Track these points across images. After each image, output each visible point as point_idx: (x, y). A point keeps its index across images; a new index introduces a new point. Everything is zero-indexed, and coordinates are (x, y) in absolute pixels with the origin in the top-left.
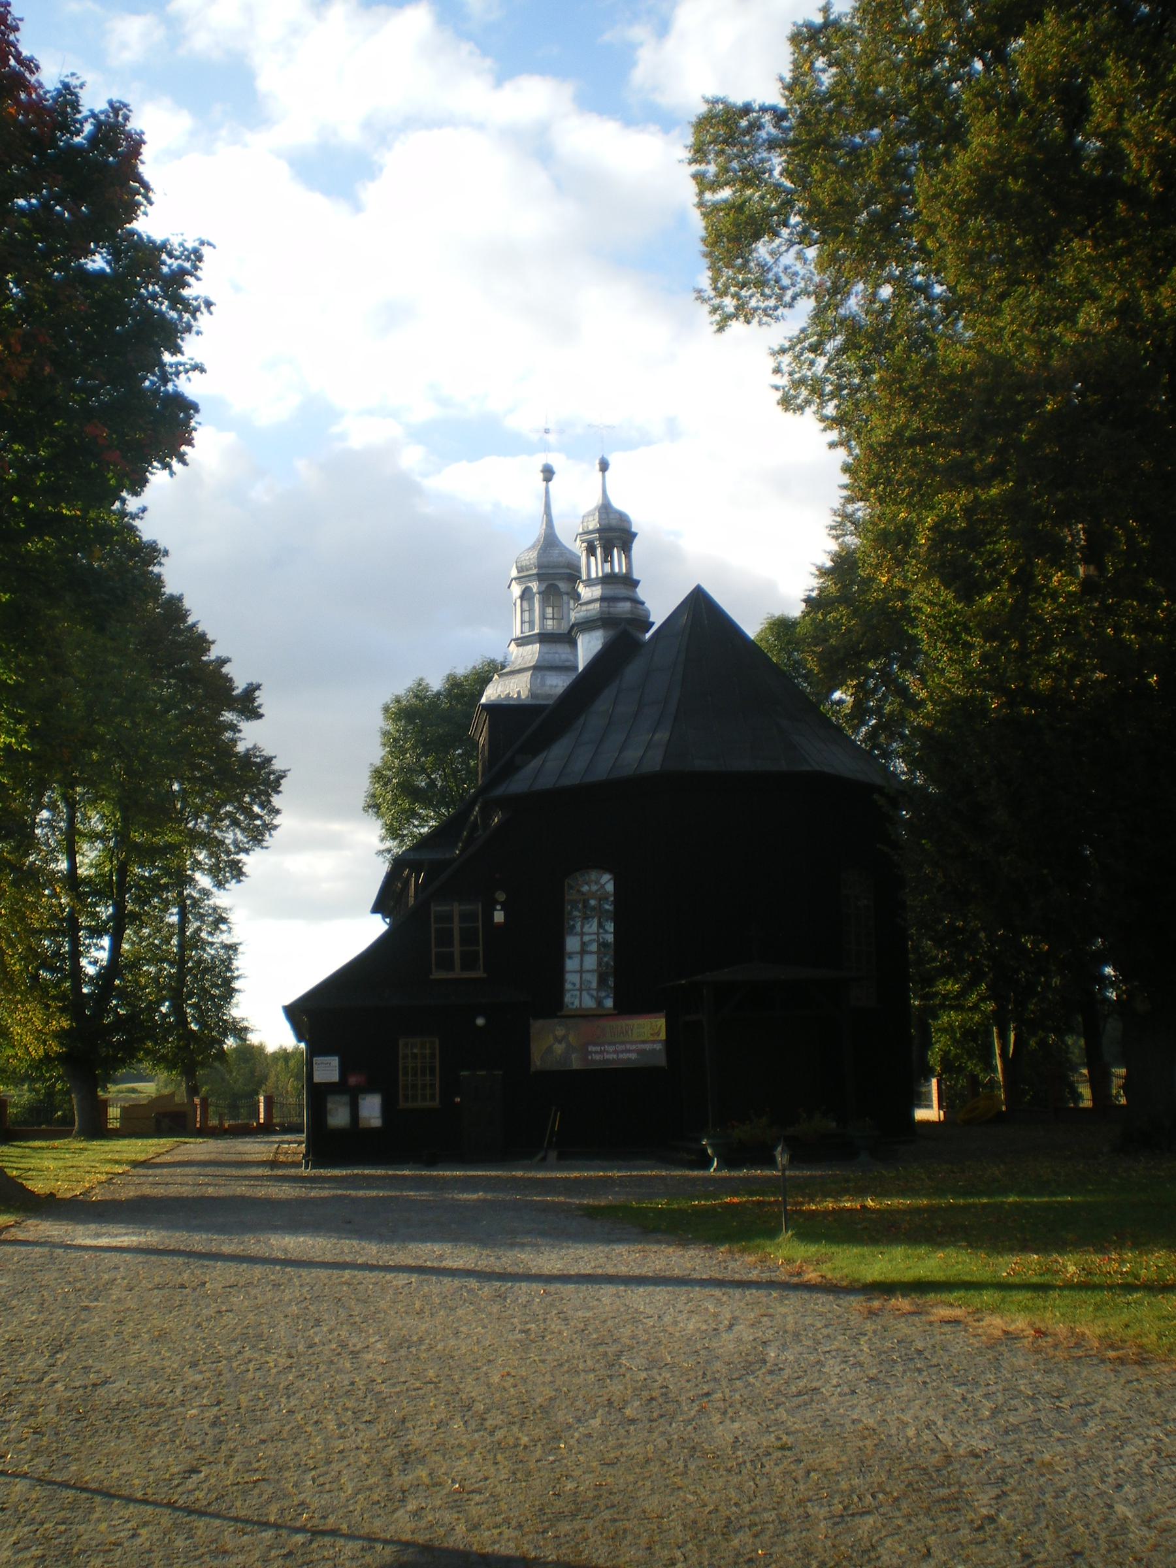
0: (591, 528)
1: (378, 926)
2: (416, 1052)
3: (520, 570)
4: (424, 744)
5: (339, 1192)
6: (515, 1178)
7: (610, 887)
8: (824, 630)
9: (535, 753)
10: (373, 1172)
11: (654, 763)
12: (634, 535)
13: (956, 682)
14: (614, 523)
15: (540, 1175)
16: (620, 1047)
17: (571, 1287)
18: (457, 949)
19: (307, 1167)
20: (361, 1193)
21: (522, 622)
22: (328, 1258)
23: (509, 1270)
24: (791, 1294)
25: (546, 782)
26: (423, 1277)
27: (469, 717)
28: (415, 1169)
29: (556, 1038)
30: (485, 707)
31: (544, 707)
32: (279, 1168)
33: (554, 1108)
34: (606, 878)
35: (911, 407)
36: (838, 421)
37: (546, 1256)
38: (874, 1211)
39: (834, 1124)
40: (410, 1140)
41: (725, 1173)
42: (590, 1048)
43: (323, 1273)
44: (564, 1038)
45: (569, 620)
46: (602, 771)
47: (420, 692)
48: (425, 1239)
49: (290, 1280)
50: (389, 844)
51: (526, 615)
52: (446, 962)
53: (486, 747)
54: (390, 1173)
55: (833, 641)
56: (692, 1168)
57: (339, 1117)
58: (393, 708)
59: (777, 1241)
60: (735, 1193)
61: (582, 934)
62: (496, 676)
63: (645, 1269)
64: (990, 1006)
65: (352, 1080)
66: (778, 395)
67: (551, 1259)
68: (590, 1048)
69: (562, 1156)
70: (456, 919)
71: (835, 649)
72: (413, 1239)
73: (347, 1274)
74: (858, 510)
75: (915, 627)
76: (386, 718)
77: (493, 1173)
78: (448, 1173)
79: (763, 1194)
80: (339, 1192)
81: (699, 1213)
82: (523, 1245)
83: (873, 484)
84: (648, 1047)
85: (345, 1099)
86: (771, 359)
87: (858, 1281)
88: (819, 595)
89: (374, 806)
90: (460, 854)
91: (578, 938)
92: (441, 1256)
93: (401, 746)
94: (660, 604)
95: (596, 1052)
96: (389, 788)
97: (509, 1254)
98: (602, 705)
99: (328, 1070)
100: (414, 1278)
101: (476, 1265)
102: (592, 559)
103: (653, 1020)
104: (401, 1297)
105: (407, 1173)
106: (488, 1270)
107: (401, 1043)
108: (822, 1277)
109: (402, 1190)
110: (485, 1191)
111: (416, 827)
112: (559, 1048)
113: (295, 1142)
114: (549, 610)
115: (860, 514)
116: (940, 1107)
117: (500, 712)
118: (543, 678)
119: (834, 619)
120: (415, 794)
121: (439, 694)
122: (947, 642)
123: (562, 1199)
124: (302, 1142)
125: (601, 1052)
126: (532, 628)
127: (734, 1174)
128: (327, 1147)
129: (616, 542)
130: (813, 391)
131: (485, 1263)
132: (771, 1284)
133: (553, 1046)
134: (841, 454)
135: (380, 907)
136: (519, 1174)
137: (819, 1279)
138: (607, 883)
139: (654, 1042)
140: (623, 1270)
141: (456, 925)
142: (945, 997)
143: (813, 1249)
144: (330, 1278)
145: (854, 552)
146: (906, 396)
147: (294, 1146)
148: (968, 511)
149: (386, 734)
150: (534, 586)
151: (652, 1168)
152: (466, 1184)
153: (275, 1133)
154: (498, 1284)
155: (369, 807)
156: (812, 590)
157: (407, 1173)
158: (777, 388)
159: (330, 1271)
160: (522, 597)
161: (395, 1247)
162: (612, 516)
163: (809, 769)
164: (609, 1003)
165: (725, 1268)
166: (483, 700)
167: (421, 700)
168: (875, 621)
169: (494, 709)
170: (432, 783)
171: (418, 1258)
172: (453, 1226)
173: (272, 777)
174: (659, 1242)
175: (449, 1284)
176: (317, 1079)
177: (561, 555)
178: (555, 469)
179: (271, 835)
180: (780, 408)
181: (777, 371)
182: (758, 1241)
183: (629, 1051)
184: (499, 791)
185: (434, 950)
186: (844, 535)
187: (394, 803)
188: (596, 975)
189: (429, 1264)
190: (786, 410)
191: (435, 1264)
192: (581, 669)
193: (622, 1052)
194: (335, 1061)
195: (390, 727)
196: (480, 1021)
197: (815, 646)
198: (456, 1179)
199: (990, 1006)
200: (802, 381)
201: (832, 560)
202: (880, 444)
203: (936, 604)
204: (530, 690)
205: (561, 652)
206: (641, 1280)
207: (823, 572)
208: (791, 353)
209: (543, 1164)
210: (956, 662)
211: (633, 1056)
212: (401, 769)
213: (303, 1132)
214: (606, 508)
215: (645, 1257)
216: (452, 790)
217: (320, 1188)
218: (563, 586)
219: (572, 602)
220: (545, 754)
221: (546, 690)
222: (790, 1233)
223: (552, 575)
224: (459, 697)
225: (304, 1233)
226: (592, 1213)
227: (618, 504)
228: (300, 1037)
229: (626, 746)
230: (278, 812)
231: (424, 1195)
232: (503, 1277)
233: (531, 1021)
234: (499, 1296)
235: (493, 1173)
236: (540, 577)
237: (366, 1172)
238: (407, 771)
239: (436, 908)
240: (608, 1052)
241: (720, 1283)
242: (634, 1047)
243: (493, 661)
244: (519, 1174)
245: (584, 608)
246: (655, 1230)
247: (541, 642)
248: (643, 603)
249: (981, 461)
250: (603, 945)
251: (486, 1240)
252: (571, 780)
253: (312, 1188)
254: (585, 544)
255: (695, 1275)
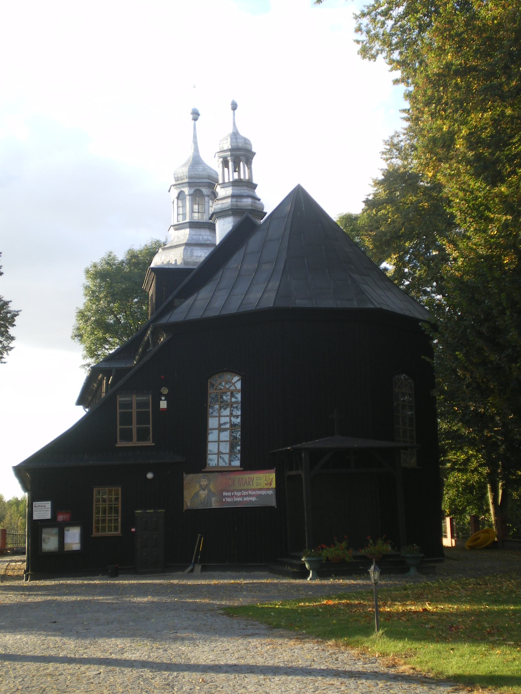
0: (225, 148)
1: (81, 412)
2: (106, 497)
3: (177, 179)
4: (113, 295)
5: (49, 598)
6: (173, 585)
7: (239, 385)
8: (377, 221)
9: (186, 297)
10: (73, 582)
11: (269, 301)
12: (254, 154)
13: (480, 245)
14: (240, 145)
15: (190, 582)
16: (245, 493)
17: (222, 676)
18: (134, 427)
19: (27, 580)
20: (64, 598)
22: (38, 653)
23: (174, 660)
24: (394, 684)
25: (196, 314)
26: (110, 668)
27: (142, 277)
28: (103, 580)
29: (201, 486)
30: (153, 269)
31: (192, 270)
32: (7, 580)
33: (199, 535)
34: (236, 378)
35: (457, 48)
36: (403, 64)
37: (200, 649)
38: (433, 614)
39: (390, 548)
40: (101, 559)
41: (317, 582)
42: (225, 494)
43: (32, 666)
44: (207, 486)
45: (209, 213)
46: (233, 308)
47: (109, 261)
48: (110, 635)
49: (7, 672)
51: (181, 210)
52: (127, 435)
53: (154, 296)
54: (86, 582)
55: (382, 229)
56: (295, 578)
57: (50, 543)
58: (92, 270)
59: (371, 637)
60: (329, 598)
61: (220, 416)
62: (160, 250)
63: (277, 660)
64: (485, 470)
65: (60, 518)
66: (359, 47)
68: (225, 494)
69: (204, 569)
70: (134, 406)
71: (384, 234)
72: (102, 635)
73: (51, 667)
74: (401, 141)
75: (451, 207)
76: (88, 278)
77: (158, 582)
78: (126, 582)
79: (349, 598)
80: (49, 598)
81: (307, 612)
82: (183, 639)
83: (427, 104)
84: (263, 493)
85: (55, 531)
86: (354, 21)
87: (441, 673)
88: (374, 198)
89: (79, 336)
91: (217, 419)
92: (123, 649)
93: (97, 296)
94: (270, 198)
95: (228, 496)
97: (173, 646)
98: (234, 263)
99: (43, 511)
100: (103, 669)
101: (149, 657)
102: (226, 170)
103: (267, 475)
104: (92, 687)
105: (97, 582)
106: (158, 661)
107: (95, 490)
108: (413, 669)
109: (93, 595)
110: (153, 596)
111: (107, 349)
112: (203, 494)
113: (21, 561)
114: (196, 207)
115: (402, 144)
116: (452, 537)
117: (164, 274)
118: (191, 252)
119: (383, 214)
120: (107, 328)
121: (122, 262)
122: (474, 217)
123: (207, 601)
125: (232, 496)
126: (184, 218)
128: (43, 565)
129: (242, 158)
130: (384, 42)
132: (375, 675)
133: (200, 493)
134: (402, 88)
135: (81, 401)
136: (175, 582)
137: (411, 671)
138: (237, 383)
139: (268, 489)
140: (260, 661)
141: (134, 411)
142: (454, 463)
143: (400, 645)
145: (399, 169)
146: (453, 40)
147: (18, 564)
149: (87, 288)
150: (186, 190)
151: (267, 577)
152: (140, 591)
153: (7, 555)
154: (166, 673)
155: (76, 336)
156: (369, 195)
157: (97, 582)
158: (358, 42)
159: (38, 664)
160: (178, 198)
161: (88, 642)
162: (239, 140)
163: (372, 306)
164: (237, 463)
165: (337, 660)
166: (152, 265)
167: (111, 266)
168: (411, 215)
169: (159, 271)
170: (118, 321)
171: (105, 651)
172: (131, 623)
174: (282, 636)
175: (130, 673)
176: (35, 517)
177: (204, 170)
178: (200, 112)
180: (360, 56)
181: (359, 30)
182: (357, 638)
183: (249, 496)
184: (164, 320)
185: (119, 427)
187: (93, 333)
188: (228, 443)
189: (113, 656)
190: (364, 57)
191: (118, 657)
192: (218, 242)
193: (246, 496)
194: (48, 505)
195: (89, 283)
196: (150, 476)
197: (371, 231)
199: (485, 470)
200: (376, 36)
201: (383, 175)
202: (435, 75)
204: (183, 259)
205: (204, 235)
206: (275, 671)
207: (378, 183)
208: (368, 17)
209: (191, 575)
210: (479, 230)
211: (253, 499)
212: (97, 311)
213: (24, 554)
214: (235, 135)
215: (274, 649)
216: (131, 326)
217: (36, 595)
218: (205, 191)
219: (211, 202)
220: (194, 297)
221: (194, 259)
222: (381, 632)
223: (199, 185)
224: (136, 265)
225: (20, 632)
227: (243, 133)
228: (25, 488)
229: (250, 291)
230: (13, 338)
233: (184, 475)
234: (168, 684)
235: (158, 582)
236: (190, 184)
237: (69, 582)
238: (102, 312)
239: (120, 399)
240: (236, 496)
242: (254, 493)
243: (158, 241)
244: (175, 582)
245: (220, 202)
246: (278, 626)
248: (259, 200)
249: (508, 84)
250: (233, 426)
251: (153, 635)
253: (30, 595)
254: (221, 159)
255: (315, 666)
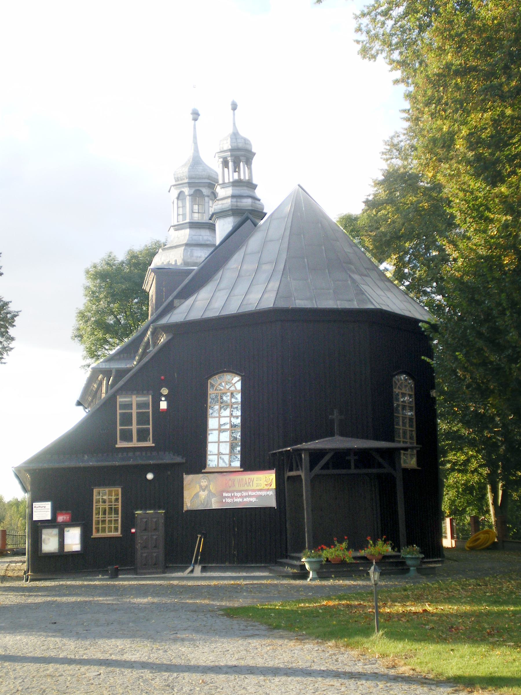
0: (225, 148)
1: (80, 414)
2: (106, 498)
4: (113, 295)
5: (49, 599)
8: (377, 222)
10: (73, 583)
12: (254, 154)
13: (480, 245)
14: (240, 145)
16: (245, 494)
17: (222, 677)
18: (134, 427)
20: (64, 599)
21: (178, 215)
22: (38, 654)
25: (196, 315)
29: (201, 487)
33: (199, 536)
35: (457, 48)
36: (403, 64)
39: (390, 549)
40: (102, 558)
41: (318, 582)
42: (225, 494)
43: (32, 667)
44: (206, 487)
46: (233, 309)
48: (110, 636)
49: (7, 673)
50: (89, 361)
51: (181, 210)
52: (127, 436)
54: (86, 583)
55: (382, 229)
57: (50, 544)
58: (92, 271)
59: (371, 638)
60: (329, 598)
61: (219, 417)
62: (160, 250)
63: (277, 661)
65: (60, 519)
66: (359, 47)
67: (205, 652)
68: (225, 494)
71: (384, 234)
72: (102, 636)
73: (51, 668)
75: (451, 207)
79: (349, 599)
80: (49, 599)
82: (183, 640)
83: (428, 104)
84: (263, 493)
85: (55, 531)
86: (354, 21)
88: (374, 198)
90: (137, 365)
93: (97, 297)
95: (228, 497)
96: (89, 323)
97: (173, 647)
98: (234, 263)
100: (103, 670)
101: (149, 658)
102: (226, 170)
103: (267, 475)
104: (92, 688)
106: (158, 662)
107: (95, 491)
108: (413, 670)
111: (107, 350)
112: (203, 495)
114: (196, 207)
115: (402, 144)
120: (107, 328)
121: (123, 262)
122: (474, 218)
123: (207, 602)
124: (24, 562)
125: (232, 497)
127: (325, 583)
129: (242, 158)
130: (384, 42)
131: (156, 655)
132: (376, 676)
133: (200, 493)
134: (402, 88)
138: (236, 383)
139: (268, 490)
140: (260, 662)
141: (134, 411)
142: (455, 464)
144: (38, 671)
145: (399, 169)
148: (496, 122)
149: (87, 288)
150: (186, 191)
155: (76, 337)
156: (369, 195)
158: (358, 42)
159: (38, 665)
160: (178, 198)
161: (88, 643)
162: (239, 141)
163: (373, 307)
164: (237, 464)
165: (337, 661)
168: (411, 215)
170: (118, 321)
171: (104, 652)
172: (131, 624)
173: (9, 316)
174: (282, 637)
175: (130, 674)
179: (8, 355)
180: (360, 56)
181: (359, 30)
182: (357, 638)
183: (249, 496)
184: (164, 321)
185: (119, 428)
186: (392, 158)
187: (93, 334)
188: (228, 444)
189: (114, 657)
190: (364, 57)
191: (118, 658)
193: (246, 497)
194: (48, 505)
195: (89, 283)
196: (150, 476)
197: (371, 232)
198: (131, 587)
201: (383, 175)
203: (467, 191)
204: (183, 260)
205: (204, 235)
206: (275, 672)
208: (368, 17)
211: (253, 500)
212: (97, 312)
214: (235, 135)
215: (274, 650)
217: (36, 596)
218: (205, 191)
221: (193, 260)
222: (381, 633)
224: (136, 265)
226: (230, 613)
227: (243, 133)
230: (13, 339)
231: (108, 600)
232: (169, 668)
233: (185, 476)
234: (168, 685)
236: (190, 185)
237: (69, 583)
238: (102, 313)
239: (121, 400)
240: (236, 497)
241: (337, 675)
242: (254, 493)
245: (220, 202)
246: (278, 627)
247: (190, 228)
248: (259, 200)
252: (211, 314)
253: (30, 596)
254: (221, 160)
255: (315, 667)
